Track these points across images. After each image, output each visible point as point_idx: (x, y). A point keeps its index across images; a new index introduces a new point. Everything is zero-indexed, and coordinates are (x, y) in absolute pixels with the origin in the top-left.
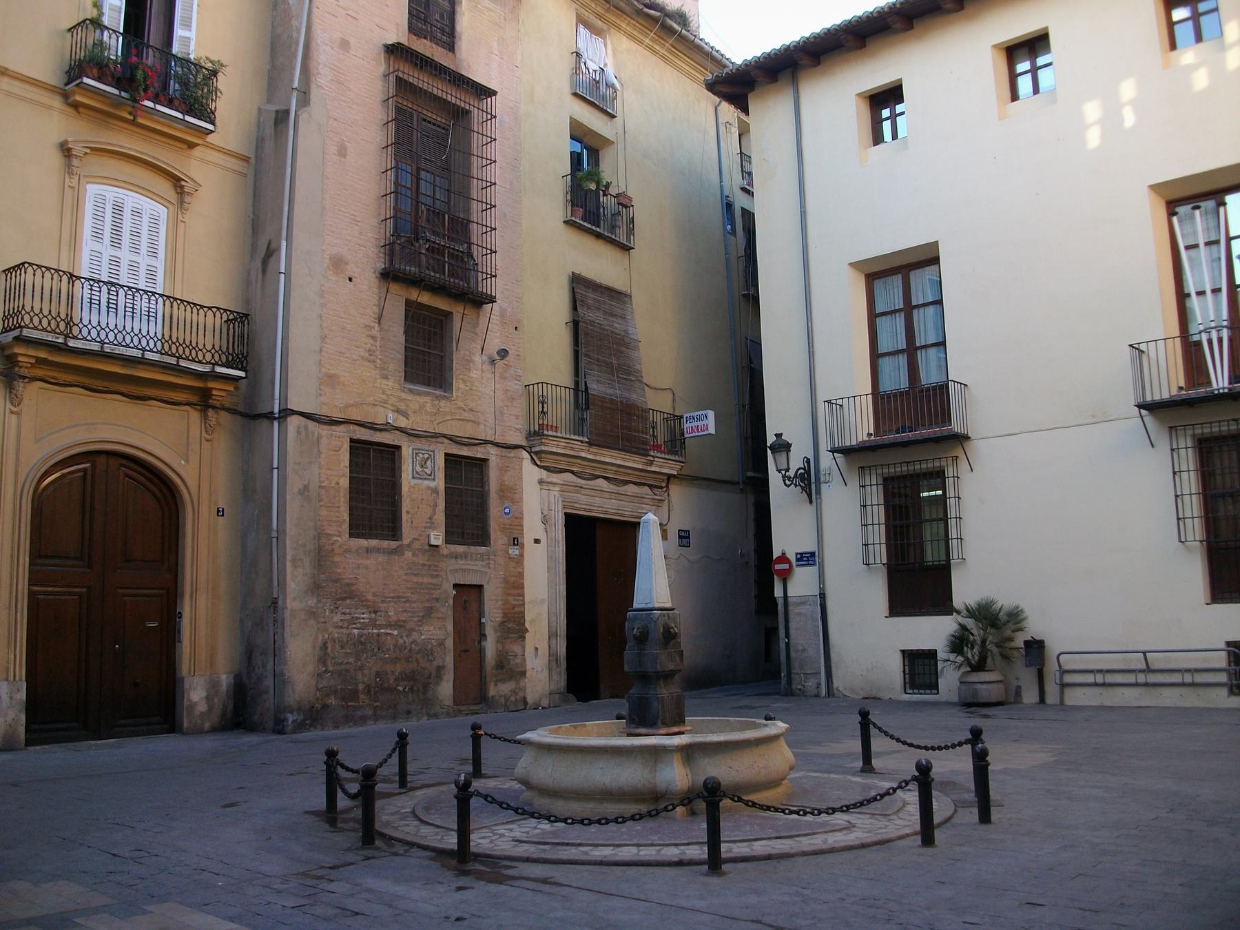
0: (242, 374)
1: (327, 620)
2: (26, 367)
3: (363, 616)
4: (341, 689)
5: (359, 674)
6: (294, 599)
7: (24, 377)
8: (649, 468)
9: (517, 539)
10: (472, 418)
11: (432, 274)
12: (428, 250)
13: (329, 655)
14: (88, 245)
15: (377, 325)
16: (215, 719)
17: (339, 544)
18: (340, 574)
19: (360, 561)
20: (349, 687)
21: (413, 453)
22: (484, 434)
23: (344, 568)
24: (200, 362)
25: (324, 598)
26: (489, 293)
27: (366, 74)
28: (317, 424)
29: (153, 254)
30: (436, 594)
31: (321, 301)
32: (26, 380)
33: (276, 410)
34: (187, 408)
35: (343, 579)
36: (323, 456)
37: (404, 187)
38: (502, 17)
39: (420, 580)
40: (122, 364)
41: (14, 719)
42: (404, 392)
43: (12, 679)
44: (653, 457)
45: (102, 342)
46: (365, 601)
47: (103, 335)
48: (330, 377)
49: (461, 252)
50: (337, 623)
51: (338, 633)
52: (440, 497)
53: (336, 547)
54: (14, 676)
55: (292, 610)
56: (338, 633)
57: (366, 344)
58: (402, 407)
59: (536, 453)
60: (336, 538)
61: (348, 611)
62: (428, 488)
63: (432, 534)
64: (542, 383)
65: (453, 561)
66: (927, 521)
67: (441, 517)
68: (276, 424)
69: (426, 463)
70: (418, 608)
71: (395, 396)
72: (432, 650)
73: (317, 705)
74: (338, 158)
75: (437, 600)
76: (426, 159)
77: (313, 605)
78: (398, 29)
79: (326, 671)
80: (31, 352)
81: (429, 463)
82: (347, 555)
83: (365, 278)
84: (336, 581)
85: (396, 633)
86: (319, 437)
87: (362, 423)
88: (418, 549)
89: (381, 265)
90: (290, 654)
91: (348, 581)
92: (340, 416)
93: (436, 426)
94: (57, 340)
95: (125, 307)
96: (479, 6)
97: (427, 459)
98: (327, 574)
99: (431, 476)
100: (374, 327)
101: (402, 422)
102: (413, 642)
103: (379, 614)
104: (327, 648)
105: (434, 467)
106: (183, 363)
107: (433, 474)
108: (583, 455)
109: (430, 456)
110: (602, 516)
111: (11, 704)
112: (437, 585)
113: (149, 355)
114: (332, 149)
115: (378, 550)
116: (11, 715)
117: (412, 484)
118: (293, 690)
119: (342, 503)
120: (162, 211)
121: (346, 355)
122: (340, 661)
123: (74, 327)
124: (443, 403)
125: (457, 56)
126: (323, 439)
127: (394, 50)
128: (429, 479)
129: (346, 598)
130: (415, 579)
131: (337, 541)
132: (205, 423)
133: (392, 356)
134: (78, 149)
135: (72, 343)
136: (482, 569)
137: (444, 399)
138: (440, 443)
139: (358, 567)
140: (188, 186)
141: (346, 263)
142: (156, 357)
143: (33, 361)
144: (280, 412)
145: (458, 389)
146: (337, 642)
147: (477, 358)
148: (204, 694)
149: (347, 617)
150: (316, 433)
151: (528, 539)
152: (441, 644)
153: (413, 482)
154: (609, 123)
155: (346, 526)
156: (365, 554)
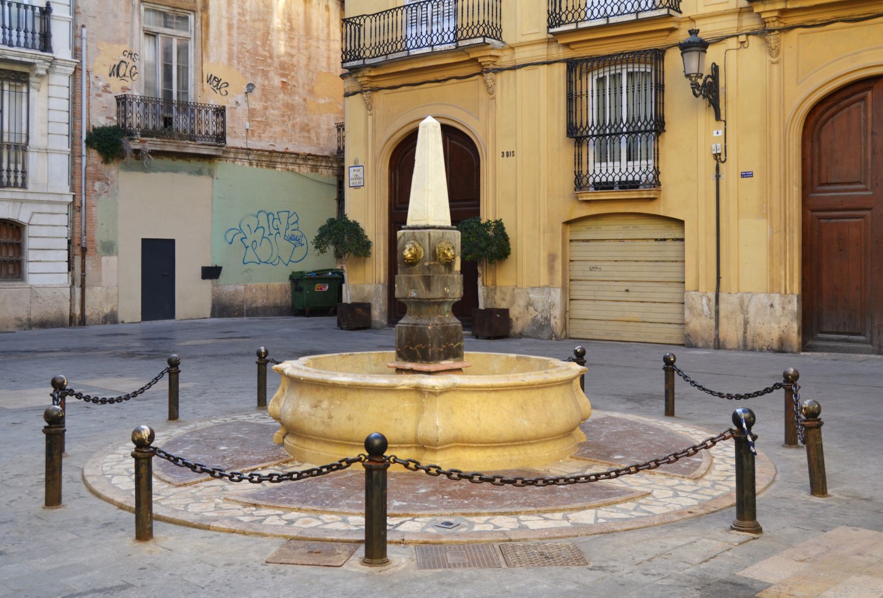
2: (773, 22)
7: (773, 31)
32: (777, 32)
41: (786, 326)
54: (786, 290)
66: (639, 66)
106: (390, 57)
111: (783, 313)
116: (784, 322)
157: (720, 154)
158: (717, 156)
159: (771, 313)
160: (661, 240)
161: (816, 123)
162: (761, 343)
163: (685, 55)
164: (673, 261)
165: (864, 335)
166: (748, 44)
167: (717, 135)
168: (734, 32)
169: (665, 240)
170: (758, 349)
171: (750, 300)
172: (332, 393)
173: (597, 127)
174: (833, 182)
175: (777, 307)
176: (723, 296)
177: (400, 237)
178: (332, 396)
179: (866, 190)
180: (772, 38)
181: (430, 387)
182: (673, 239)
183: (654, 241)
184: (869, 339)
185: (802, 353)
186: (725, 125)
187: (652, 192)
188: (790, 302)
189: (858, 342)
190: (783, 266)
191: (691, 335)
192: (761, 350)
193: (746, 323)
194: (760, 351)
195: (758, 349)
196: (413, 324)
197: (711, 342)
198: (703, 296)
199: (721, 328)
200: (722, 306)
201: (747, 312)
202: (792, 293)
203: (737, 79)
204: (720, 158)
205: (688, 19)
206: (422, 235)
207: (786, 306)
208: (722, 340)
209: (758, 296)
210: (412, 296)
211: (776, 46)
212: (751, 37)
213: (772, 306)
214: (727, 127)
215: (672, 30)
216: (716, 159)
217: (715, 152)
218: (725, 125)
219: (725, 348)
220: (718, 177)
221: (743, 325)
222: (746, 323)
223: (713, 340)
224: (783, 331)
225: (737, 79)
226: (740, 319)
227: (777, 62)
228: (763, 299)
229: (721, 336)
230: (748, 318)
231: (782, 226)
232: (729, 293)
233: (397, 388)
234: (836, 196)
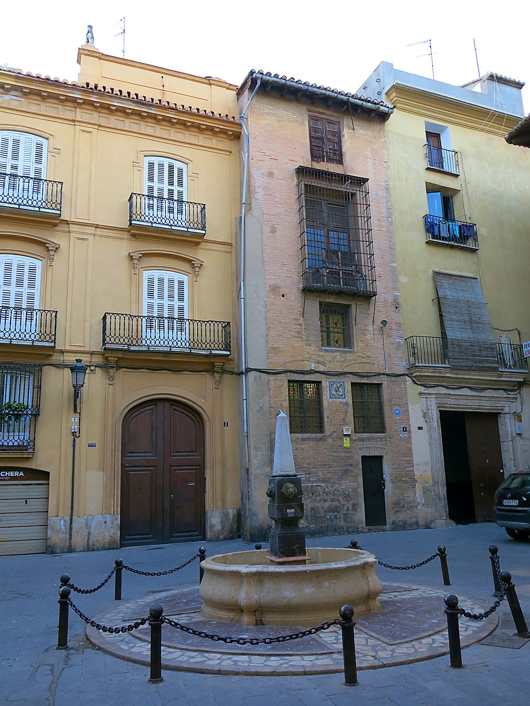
0: (228, 353)
8: (500, 379)
9: (406, 428)
10: (369, 361)
11: (332, 285)
12: (328, 273)
14: (145, 300)
15: (302, 318)
21: (329, 384)
22: (378, 370)
24: (204, 349)
26: (371, 290)
27: (286, 187)
29: (181, 299)
30: (350, 462)
33: (244, 370)
34: (204, 373)
37: (333, 244)
38: (373, 137)
39: (338, 454)
42: (321, 351)
44: (502, 372)
45: (148, 346)
46: (302, 468)
48: (274, 348)
49: (350, 271)
52: (350, 408)
54: (114, 512)
58: (321, 359)
59: (415, 377)
62: (341, 403)
63: (344, 428)
64: (412, 336)
65: (361, 443)
67: (350, 418)
68: (244, 376)
69: (338, 389)
70: (338, 470)
71: (316, 355)
72: (349, 494)
74: (271, 234)
75: (351, 465)
76: (310, 221)
78: (303, 160)
81: (340, 389)
83: (292, 294)
85: (323, 485)
88: (336, 437)
89: (301, 286)
93: (344, 368)
96: (356, 135)
97: (339, 387)
99: (343, 396)
100: (300, 319)
101: (322, 368)
102: (335, 490)
103: (311, 474)
105: (344, 391)
107: (334, 397)
108: (448, 375)
109: (341, 385)
110: (467, 410)
112: (351, 457)
113: (174, 349)
114: (267, 229)
115: (309, 439)
116: (112, 531)
117: (330, 401)
118: (258, 519)
120: (185, 278)
124: (348, 355)
125: (344, 165)
127: (301, 171)
128: (341, 398)
130: (335, 454)
133: (313, 333)
134: (136, 256)
135: (132, 348)
136: (382, 446)
137: (348, 353)
138: (348, 377)
140: (197, 263)
141: (280, 288)
142: (178, 350)
144: (245, 370)
145: (358, 346)
147: (370, 328)
148: (220, 520)
151: (414, 428)
152: (355, 490)
153: (331, 400)
154: (455, 180)
157: (76, 432)
158: (74, 433)
159: (105, 527)
175: (109, 523)
185: (122, 548)
192: (98, 550)
193: (89, 534)
200: (74, 524)
207: (114, 522)
213: (105, 522)
214: (81, 417)
216: (74, 436)
217: (73, 431)
220: (74, 446)
222: (89, 534)
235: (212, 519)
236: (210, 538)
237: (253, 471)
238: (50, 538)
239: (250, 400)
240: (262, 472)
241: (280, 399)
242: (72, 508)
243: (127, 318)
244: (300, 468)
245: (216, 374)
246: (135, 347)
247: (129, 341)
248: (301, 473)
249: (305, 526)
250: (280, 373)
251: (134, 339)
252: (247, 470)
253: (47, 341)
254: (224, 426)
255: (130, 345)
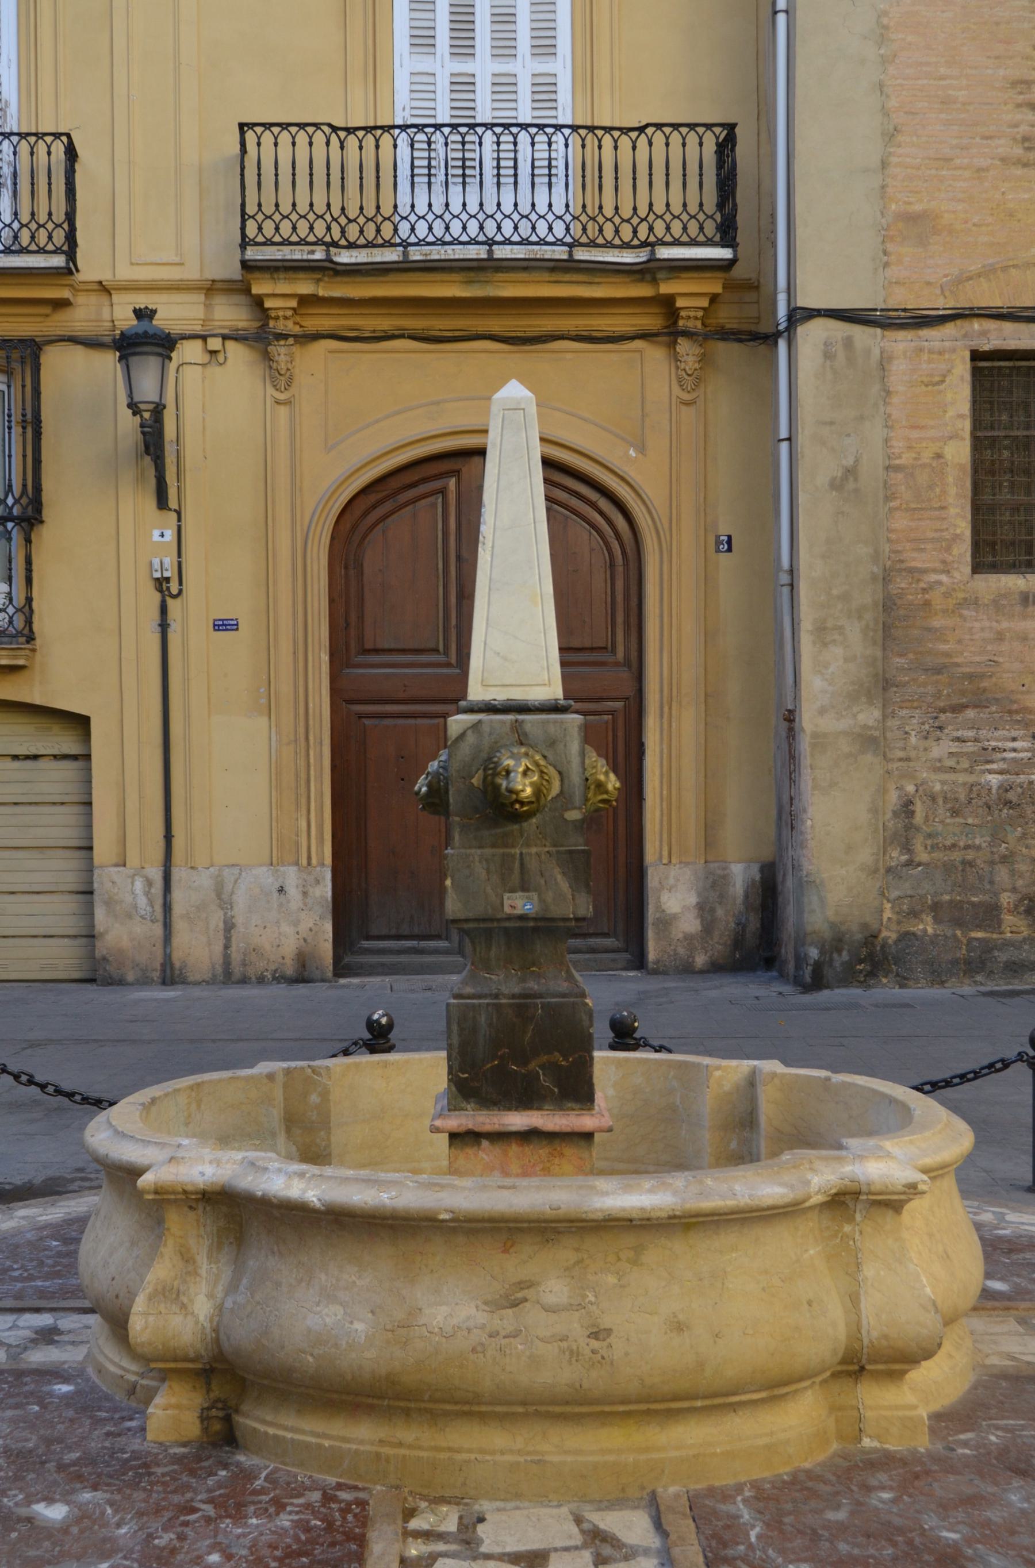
1: (913, 754)
2: (286, 318)
3: (1015, 745)
4: (951, 902)
5: (1002, 874)
6: (822, 711)
7: (285, 337)
13: (918, 829)
16: (719, 945)
17: (943, 589)
18: (948, 655)
19: (1005, 625)
20: (974, 899)
23: (960, 642)
25: (902, 708)
28: (879, 331)
29: (544, 48)
31: (882, 51)
32: (291, 341)
34: (638, 344)
35: (957, 665)
36: (895, 400)
40: (461, 279)
41: (311, 930)
43: (304, 862)
46: (1017, 712)
47: (490, 227)
48: (911, 219)
50: (940, 760)
51: (943, 783)
53: (936, 597)
54: (309, 858)
55: (815, 735)
56: (943, 783)
57: (1016, 126)
60: (933, 577)
61: (970, 734)
68: (782, 344)
73: (884, 934)
77: (871, 723)
79: (909, 863)
80: (283, 288)
82: (966, 612)
84: (938, 670)
86: (884, 363)
87: (1005, 311)
90: (812, 826)
91: (968, 670)
92: (941, 303)
94: (311, 257)
95: (413, 167)
98: (911, 656)
104: (913, 813)
111: (305, 904)
113: (502, 252)
116: (308, 921)
118: (822, 900)
119: (951, 500)
121: (958, 161)
122: (948, 843)
123: (61, 221)
126: (895, 362)
129: (965, 706)
131: (940, 583)
132: (678, 368)
139: (1000, 637)
142: (519, 252)
143: (294, 303)
146: (940, 801)
148: (692, 899)
149: (970, 747)
150: (876, 352)
155: (963, 550)
156: (1018, 608)
157: (168, 580)
158: (161, 584)
159: (281, 905)
160: (27, 757)
161: (354, 527)
162: (261, 965)
163: (134, 360)
164: (54, 803)
165: (447, 938)
166: (226, 358)
167: (160, 539)
168: (198, 329)
169: (36, 757)
170: (254, 979)
171: (236, 881)
172: (577, 1250)
173: (21, 497)
174: (386, 646)
175: (293, 892)
176: (178, 874)
177: (462, 736)
178: (580, 1261)
179: (448, 665)
180: (280, 351)
181: (900, 1188)
182: (55, 756)
183: (9, 759)
184: (456, 945)
185: (342, 981)
186: (179, 520)
187: (23, 653)
188: (318, 882)
189: (436, 952)
190: (304, 811)
191: (110, 959)
192: (261, 980)
193: (229, 927)
194: (259, 983)
195: (254, 979)
196: (514, 996)
197: (155, 970)
198: (135, 875)
199: (177, 941)
200: (178, 895)
201: (231, 904)
202: (323, 865)
203: (204, 428)
204: (168, 588)
205: (96, 287)
206: (551, 729)
207: (311, 890)
208: (177, 964)
209: (254, 872)
210: (519, 911)
211: (288, 369)
212: (230, 345)
213: (281, 890)
214: (183, 523)
215: (61, 304)
216: (161, 591)
217: (158, 575)
218: (179, 520)
219: (184, 982)
220: (164, 626)
221: (222, 933)
222: (229, 927)
223: (159, 968)
224: (305, 940)
225: (204, 428)
226: (217, 919)
227: (287, 403)
228: (265, 877)
229: (177, 957)
230: (233, 917)
231: (301, 730)
232: (192, 868)
233: (807, 1204)
234: (422, 674)
235: (665, 897)
236: (657, 962)
237: (808, 720)
238: (102, 935)
239: (803, 439)
240: (844, 724)
241: (931, 433)
242: (168, 837)
243: (319, 138)
244: (1010, 712)
245: (684, 346)
246: (354, 252)
247: (329, 228)
248: (1014, 734)
249: (1019, 937)
250: (943, 319)
251: (350, 221)
252: (790, 717)
253: (41, 251)
254: (718, 551)
255: (335, 244)
